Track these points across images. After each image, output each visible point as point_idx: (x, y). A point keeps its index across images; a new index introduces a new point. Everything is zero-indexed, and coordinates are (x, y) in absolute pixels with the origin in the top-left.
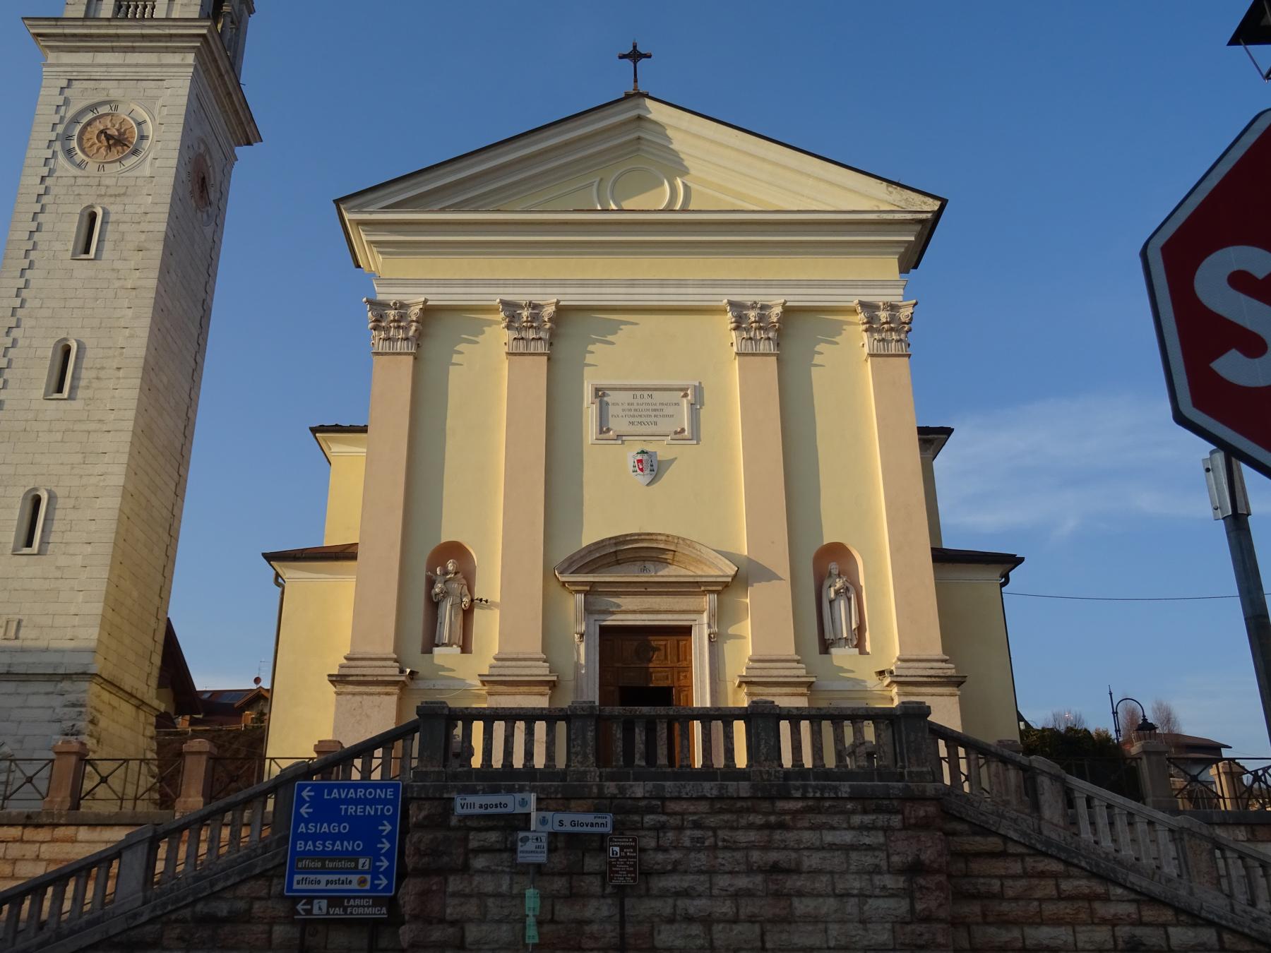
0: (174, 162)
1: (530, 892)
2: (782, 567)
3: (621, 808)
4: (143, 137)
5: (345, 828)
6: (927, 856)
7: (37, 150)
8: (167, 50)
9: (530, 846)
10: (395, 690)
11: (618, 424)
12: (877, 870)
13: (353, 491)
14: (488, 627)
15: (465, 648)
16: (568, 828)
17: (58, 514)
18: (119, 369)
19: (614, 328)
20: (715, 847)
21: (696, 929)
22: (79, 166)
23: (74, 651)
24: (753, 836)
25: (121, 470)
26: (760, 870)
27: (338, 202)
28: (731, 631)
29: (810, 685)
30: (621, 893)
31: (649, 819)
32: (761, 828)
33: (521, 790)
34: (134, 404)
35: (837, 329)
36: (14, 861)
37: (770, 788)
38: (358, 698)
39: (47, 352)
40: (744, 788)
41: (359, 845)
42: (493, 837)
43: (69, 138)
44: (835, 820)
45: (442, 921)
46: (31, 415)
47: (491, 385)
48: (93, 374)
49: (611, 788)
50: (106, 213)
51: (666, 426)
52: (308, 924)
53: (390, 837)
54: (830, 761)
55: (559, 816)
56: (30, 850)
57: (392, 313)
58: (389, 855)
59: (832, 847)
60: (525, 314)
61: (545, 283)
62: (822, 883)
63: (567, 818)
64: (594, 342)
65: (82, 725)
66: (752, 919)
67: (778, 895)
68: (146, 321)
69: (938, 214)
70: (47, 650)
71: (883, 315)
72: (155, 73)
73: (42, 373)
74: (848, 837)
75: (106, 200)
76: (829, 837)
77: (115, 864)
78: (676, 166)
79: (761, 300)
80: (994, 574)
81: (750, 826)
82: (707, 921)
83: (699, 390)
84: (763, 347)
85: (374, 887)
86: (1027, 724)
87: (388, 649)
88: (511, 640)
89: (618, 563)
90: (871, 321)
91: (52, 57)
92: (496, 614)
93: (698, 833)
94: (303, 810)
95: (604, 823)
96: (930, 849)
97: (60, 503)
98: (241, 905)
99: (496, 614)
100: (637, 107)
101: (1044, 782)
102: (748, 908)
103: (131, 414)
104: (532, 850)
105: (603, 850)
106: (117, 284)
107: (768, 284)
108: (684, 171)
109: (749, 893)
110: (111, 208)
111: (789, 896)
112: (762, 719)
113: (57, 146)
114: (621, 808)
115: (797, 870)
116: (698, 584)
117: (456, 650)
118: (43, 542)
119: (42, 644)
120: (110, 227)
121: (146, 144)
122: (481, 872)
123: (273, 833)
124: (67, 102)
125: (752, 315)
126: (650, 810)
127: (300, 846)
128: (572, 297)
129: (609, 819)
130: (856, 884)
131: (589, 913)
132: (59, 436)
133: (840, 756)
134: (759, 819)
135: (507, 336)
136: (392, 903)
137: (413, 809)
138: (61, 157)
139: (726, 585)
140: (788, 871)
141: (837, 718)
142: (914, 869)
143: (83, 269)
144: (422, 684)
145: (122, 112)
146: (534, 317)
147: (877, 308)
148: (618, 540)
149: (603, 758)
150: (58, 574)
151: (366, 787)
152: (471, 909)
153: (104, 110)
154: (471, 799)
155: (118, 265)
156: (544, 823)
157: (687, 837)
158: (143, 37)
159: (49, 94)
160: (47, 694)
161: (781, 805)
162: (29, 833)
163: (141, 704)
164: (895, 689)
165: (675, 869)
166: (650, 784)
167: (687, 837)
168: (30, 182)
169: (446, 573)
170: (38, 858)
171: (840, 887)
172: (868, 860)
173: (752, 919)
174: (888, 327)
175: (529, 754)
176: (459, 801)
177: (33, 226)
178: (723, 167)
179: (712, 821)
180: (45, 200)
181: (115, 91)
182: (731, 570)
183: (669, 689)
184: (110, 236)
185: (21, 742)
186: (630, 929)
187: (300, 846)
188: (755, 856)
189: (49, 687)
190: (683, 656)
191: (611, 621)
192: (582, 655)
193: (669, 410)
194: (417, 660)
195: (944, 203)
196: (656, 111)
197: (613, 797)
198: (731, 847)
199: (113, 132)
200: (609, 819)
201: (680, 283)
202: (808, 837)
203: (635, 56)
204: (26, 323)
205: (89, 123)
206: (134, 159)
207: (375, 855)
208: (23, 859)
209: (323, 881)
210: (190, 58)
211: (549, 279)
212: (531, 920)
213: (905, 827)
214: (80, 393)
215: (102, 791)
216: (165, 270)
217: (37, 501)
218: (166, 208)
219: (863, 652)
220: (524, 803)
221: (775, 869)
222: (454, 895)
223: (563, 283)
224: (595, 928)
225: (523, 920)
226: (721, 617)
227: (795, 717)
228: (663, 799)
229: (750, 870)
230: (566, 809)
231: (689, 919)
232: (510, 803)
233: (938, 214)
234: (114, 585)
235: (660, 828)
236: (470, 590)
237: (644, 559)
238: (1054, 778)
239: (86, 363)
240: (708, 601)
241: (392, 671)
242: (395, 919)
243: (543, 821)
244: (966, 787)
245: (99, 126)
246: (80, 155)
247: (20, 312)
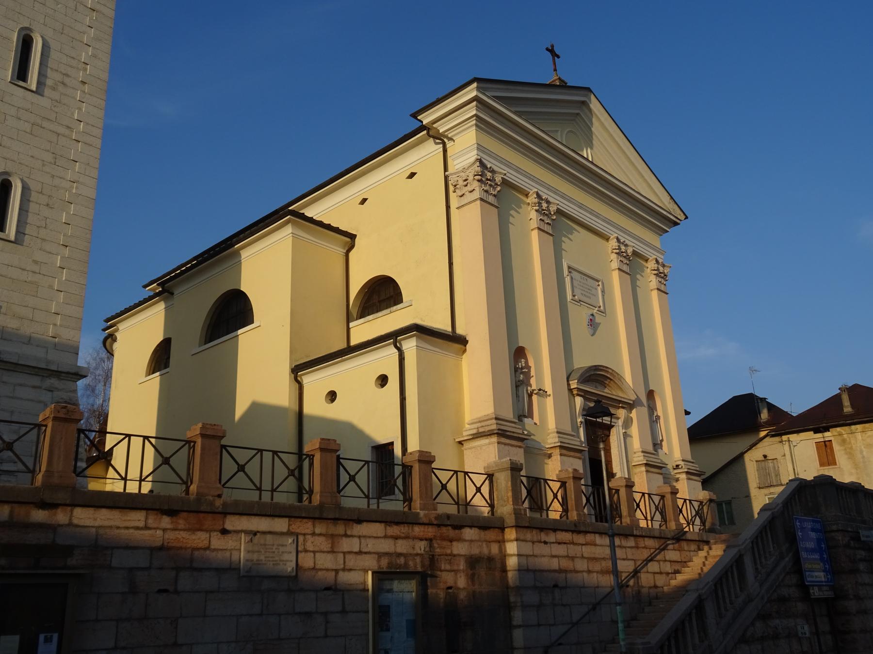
18: (84, 83)
38: (507, 447)
48: (58, 77)
97: (34, 196)
100: (586, 96)
116: (620, 402)
150: (36, 268)
160: (34, 387)
189: (35, 381)
215: (240, 480)
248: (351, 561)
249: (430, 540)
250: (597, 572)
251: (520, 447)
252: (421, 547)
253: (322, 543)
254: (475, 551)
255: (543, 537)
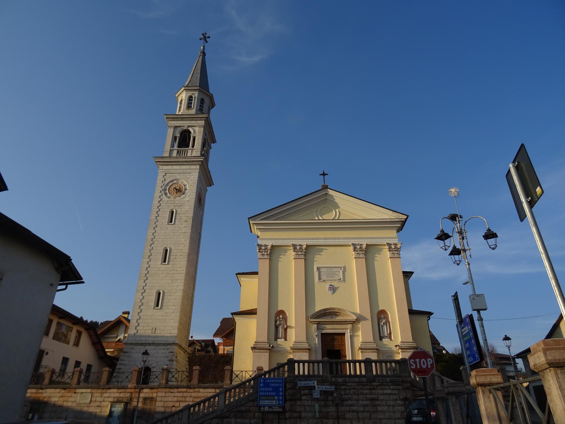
0: (194, 196)
1: (316, 405)
2: (368, 316)
3: (336, 384)
4: (186, 189)
5: (271, 389)
6: (408, 396)
7: (157, 193)
8: (192, 165)
9: (316, 394)
10: (268, 351)
11: (324, 277)
12: (396, 400)
13: (251, 292)
14: (292, 335)
15: (286, 339)
16: (324, 389)
17: (166, 297)
19: (321, 251)
20: (358, 394)
21: (355, 414)
22: (168, 198)
23: (170, 337)
24: (367, 391)
25: (182, 284)
26: (369, 400)
27: (249, 218)
28: (356, 334)
29: (377, 349)
30: (337, 405)
31: (343, 387)
32: (369, 389)
33: (313, 380)
34: (185, 266)
35: (381, 250)
36: (185, 397)
37: (369, 380)
39: (162, 251)
40: (364, 380)
41: (275, 394)
42: (307, 391)
43: (166, 190)
44: (386, 387)
45: (296, 412)
46: (157, 269)
47: (290, 267)
48: (174, 257)
49: (334, 380)
50: (176, 211)
51: (337, 278)
52: (264, 413)
53: (282, 391)
54: (385, 373)
55: (322, 387)
56: (189, 394)
57: (263, 248)
58: (282, 396)
59: (386, 394)
60: (298, 247)
61: (303, 239)
62: (384, 403)
63: (324, 387)
64: (316, 255)
65: (174, 358)
66: (368, 412)
67: (374, 406)
68: (188, 242)
69: (406, 219)
70: (163, 336)
71: (393, 247)
72: (188, 171)
73: (160, 257)
74: (389, 391)
75: (176, 207)
76: (385, 391)
77: (217, 398)
78: (336, 206)
79: (361, 243)
80: (426, 317)
81: (366, 389)
82: (357, 412)
83: (345, 268)
84: (361, 256)
85: (279, 404)
86: (447, 351)
87: (266, 340)
88: (297, 338)
89: (325, 316)
90: (390, 248)
91: (161, 167)
92: (293, 331)
93: (354, 391)
94: (261, 385)
95: (332, 388)
96: (409, 395)
97: (166, 294)
98: (247, 408)
99: (293, 331)
101: (436, 378)
102: (367, 409)
103: (185, 269)
104: (316, 395)
105: (332, 395)
106: (180, 231)
107: (362, 238)
108: (338, 207)
109: (366, 405)
110: (178, 210)
111: (376, 406)
112: (368, 362)
113: (163, 192)
114: (336, 384)
115: (378, 400)
117: (283, 340)
118: (162, 305)
119: (162, 335)
120: (177, 215)
121: (187, 191)
122: (305, 400)
123: (253, 391)
124: (165, 180)
125: (358, 247)
126: (343, 385)
127: (261, 393)
128: (310, 243)
129: (333, 387)
130: (392, 403)
131: (329, 410)
132: (165, 275)
133: (387, 372)
134: (369, 387)
135: (293, 253)
136: (283, 408)
137: (287, 385)
138: (164, 195)
139: (354, 322)
140: (376, 400)
141: (386, 362)
142: (405, 399)
143: (170, 227)
144: (275, 349)
145: (180, 182)
146: (301, 248)
147: (391, 244)
148: (325, 310)
149: (331, 373)
151: (270, 379)
152: (302, 409)
153: (175, 182)
154: (301, 382)
155: (180, 226)
156: (318, 388)
157: (352, 391)
158: (185, 161)
159: (160, 177)
161: (373, 384)
162: (188, 390)
163: (185, 351)
164: (400, 350)
165: (349, 399)
166: (343, 379)
167: (352, 391)
168: (156, 203)
169: (280, 318)
170: (191, 396)
171: (388, 404)
172: (395, 397)
173: (368, 412)
174: (395, 250)
175: (314, 371)
176: (299, 383)
177: (157, 215)
178: (349, 207)
179: (357, 388)
180: (160, 207)
181: (178, 176)
182: (355, 318)
183: (339, 350)
184: (177, 217)
185: (157, 363)
186: (339, 414)
187: (261, 393)
188: (368, 396)
189: (164, 347)
190: (343, 341)
191: (324, 332)
192: (317, 341)
193: (337, 273)
194: (273, 343)
195: (408, 216)
196: (331, 192)
197: (334, 382)
198: (362, 394)
199: (178, 188)
200: (333, 387)
201: (339, 238)
202: (380, 391)
203: (324, 174)
204: (155, 243)
205: (171, 186)
206: (183, 196)
207: (278, 395)
208: (187, 397)
209: (267, 402)
210: (198, 167)
211: (304, 238)
212: (317, 411)
213: (403, 389)
214: (171, 263)
215: (173, 379)
216: (192, 226)
217: (159, 294)
218: (193, 210)
219: (391, 340)
220: (314, 383)
221: (373, 399)
222: (298, 405)
223: (308, 239)
224: (331, 413)
225: (315, 412)
226: (353, 330)
227: (376, 362)
228: (346, 382)
229: (367, 400)
230: (324, 385)
231: (353, 411)
232: (310, 383)
233: (406, 219)
234: (181, 318)
235: (345, 389)
236: (286, 323)
237: (332, 315)
238: (438, 377)
239: (172, 254)
240: (349, 326)
241: (267, 346)
242: (284, 411)
243: (318, 388)
244: (418, 379)
245: (174, 186)
246: (169, 195)
247: (154, 240)
248: (106, 399)
249: (131, 393)
250: (296, 412)
251: (481, 319)
252: (128, 395)
253: (99, 395)
254: (147, 396)
255: (171, 390)
